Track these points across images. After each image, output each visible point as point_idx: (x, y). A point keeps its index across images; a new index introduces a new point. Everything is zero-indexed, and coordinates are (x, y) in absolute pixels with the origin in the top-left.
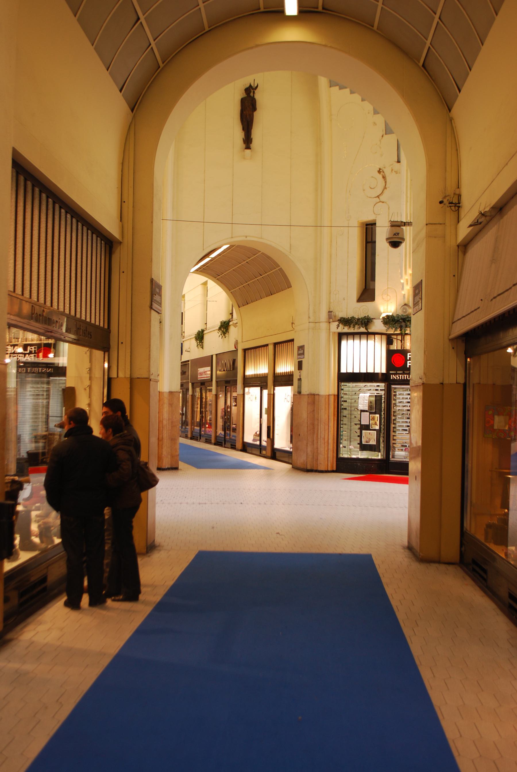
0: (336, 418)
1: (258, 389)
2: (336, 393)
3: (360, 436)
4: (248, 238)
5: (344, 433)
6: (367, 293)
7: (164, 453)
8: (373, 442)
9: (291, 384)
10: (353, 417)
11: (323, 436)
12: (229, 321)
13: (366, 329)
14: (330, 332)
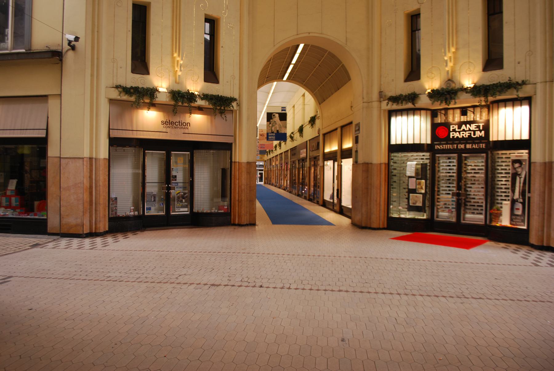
0: (387, 184)
1: (332, 161)
2: (387, 162)
3: (408, 199)
4: (311, 35)
5: (394, 194)
6: (413, 72)
7: (243, 212)
8: (420, 204)
9: (351, 157)
10: (402, 182)
12: (315, 116)
13: (413, 104)
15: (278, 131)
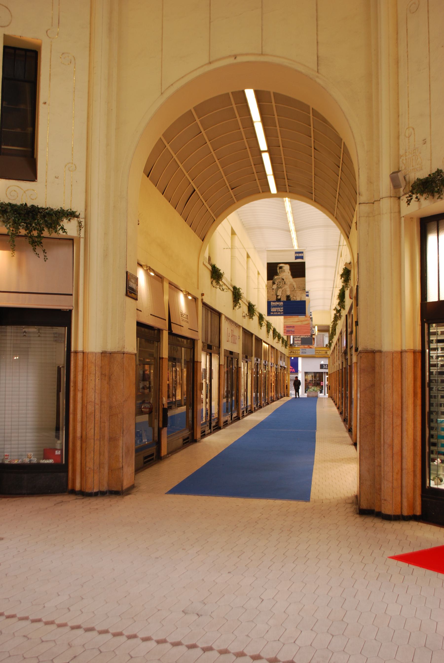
2: (418, 347)
4: (240, 59)
11: (389, 441)
14: (400, 218)
15: (288, 297)
